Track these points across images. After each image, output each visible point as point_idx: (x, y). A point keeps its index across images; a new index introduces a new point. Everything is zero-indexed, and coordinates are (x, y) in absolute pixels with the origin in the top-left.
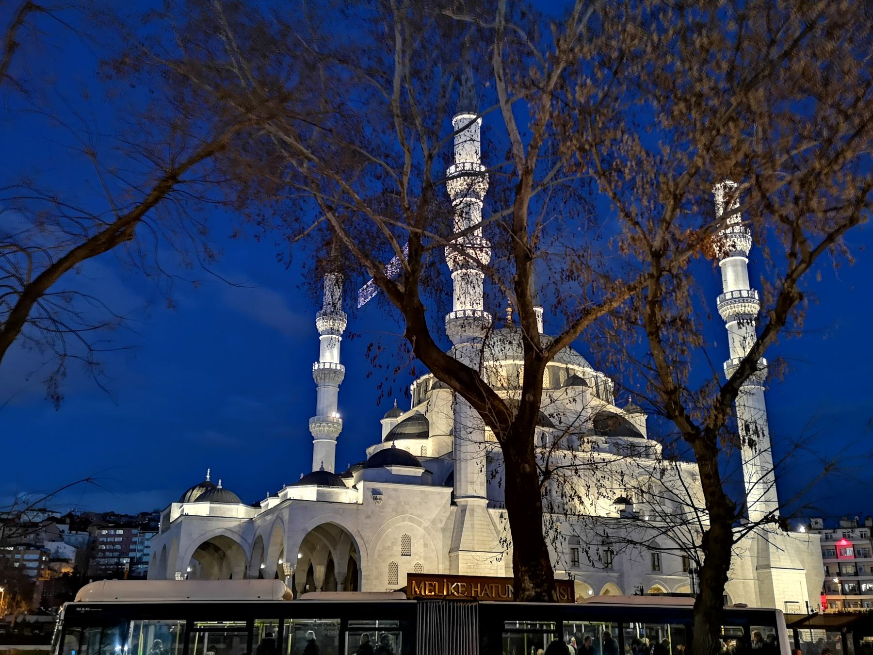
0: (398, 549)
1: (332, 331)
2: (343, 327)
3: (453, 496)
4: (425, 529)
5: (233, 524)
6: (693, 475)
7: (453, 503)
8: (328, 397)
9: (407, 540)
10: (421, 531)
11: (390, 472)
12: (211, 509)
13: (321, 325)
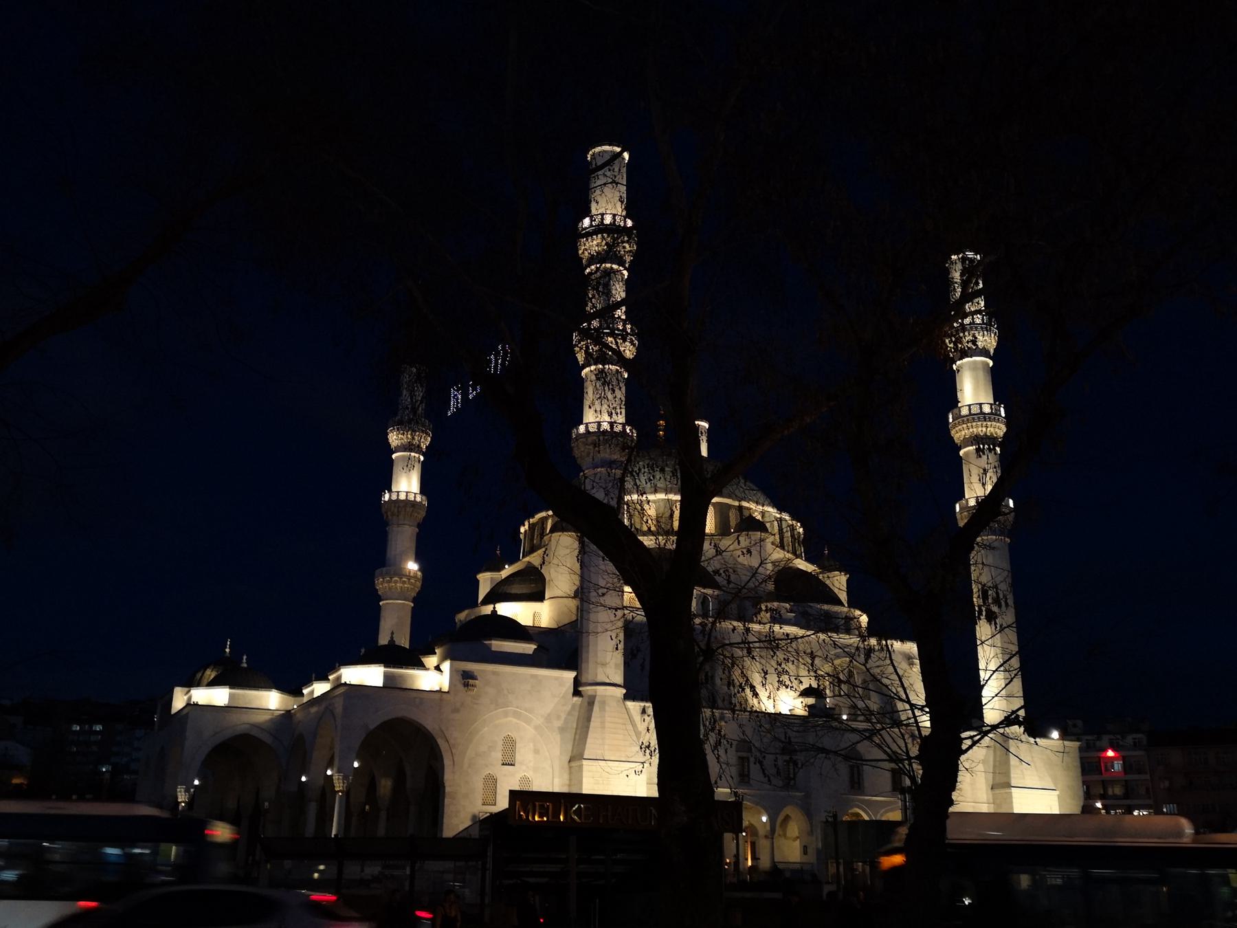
0: (498, 755)
1: (409, 447)
2: (425, 442)
3: (577, 683)
4: (536, 728)
5: (262, 718)
6: (909, 658)
7: (577, 693)
9: (510, 745)
10: (530, 731)
11: (488, 648)
12: (231, 697)
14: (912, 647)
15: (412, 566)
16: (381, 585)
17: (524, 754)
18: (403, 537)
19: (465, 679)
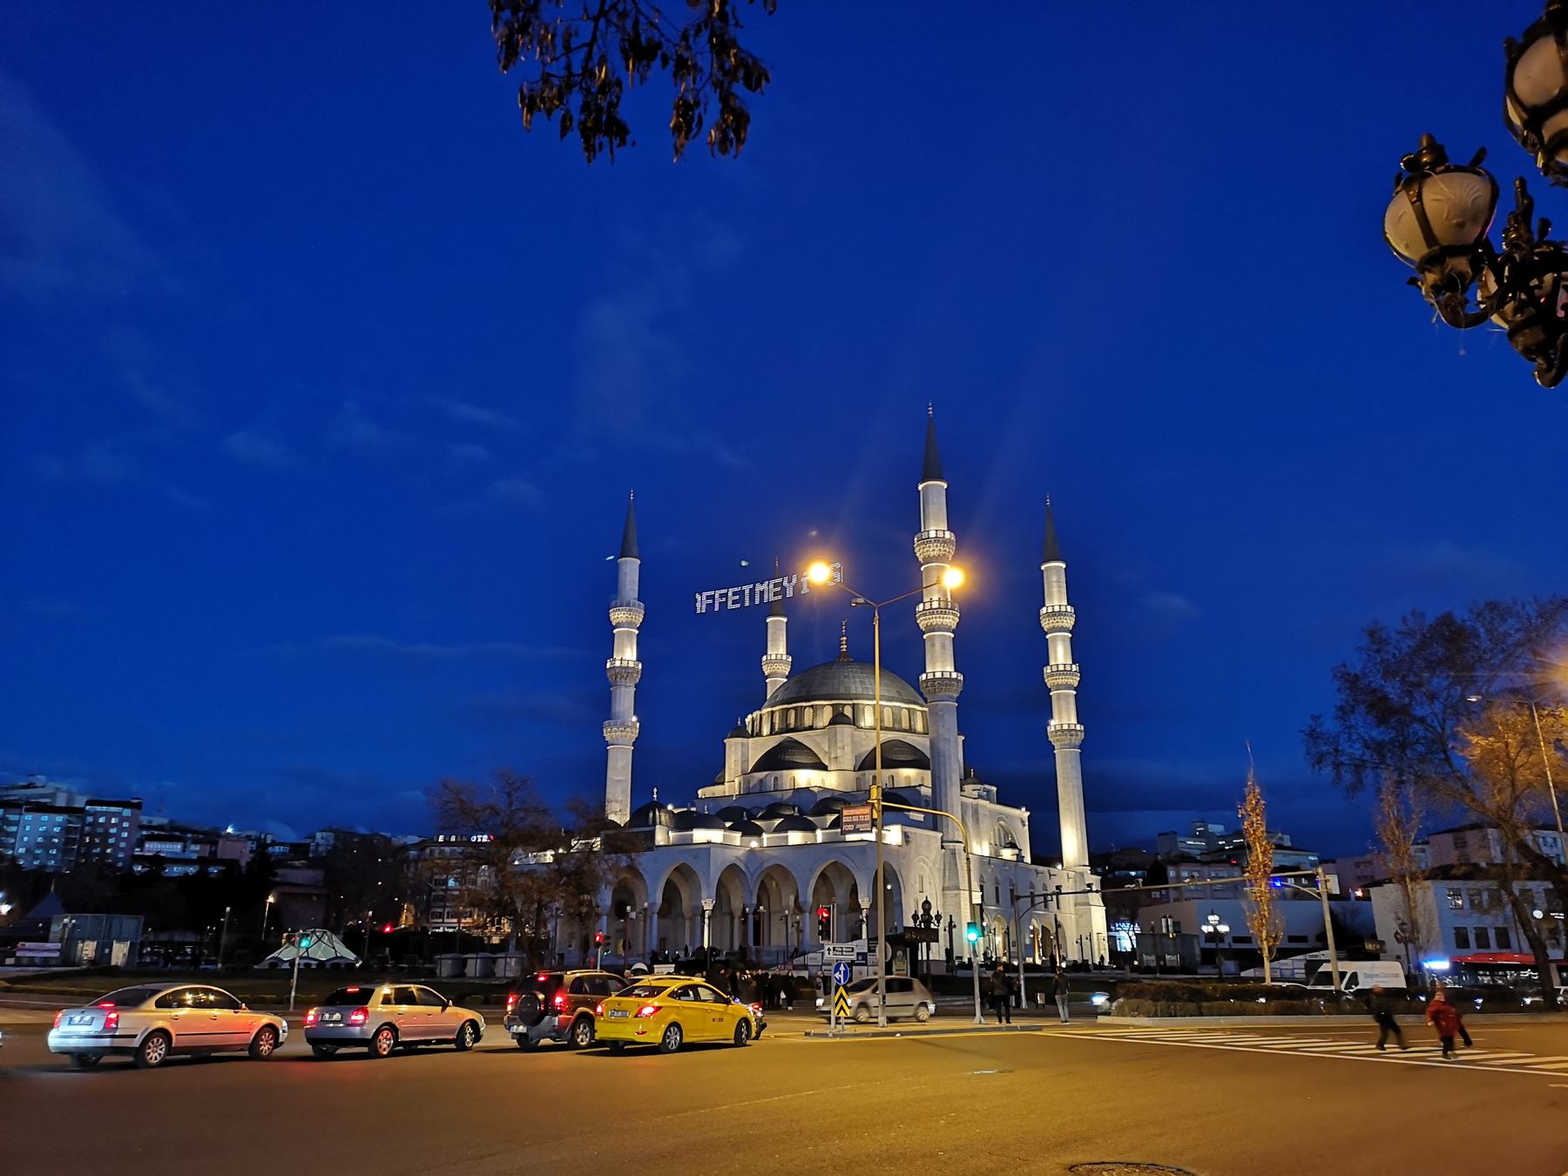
1: (630, 624)
8: (625, 699)
13: (617, 616)
14: (1024, 814)
15: (634, 719)
16: (608, 734)
17: (926, 886)
18: (625, 699)
19: (906, 836)
